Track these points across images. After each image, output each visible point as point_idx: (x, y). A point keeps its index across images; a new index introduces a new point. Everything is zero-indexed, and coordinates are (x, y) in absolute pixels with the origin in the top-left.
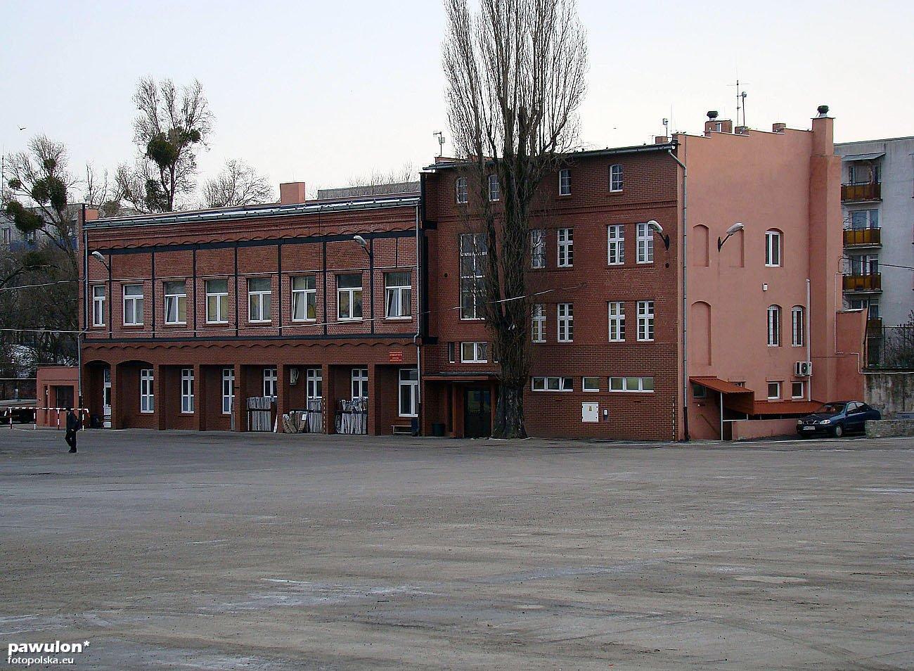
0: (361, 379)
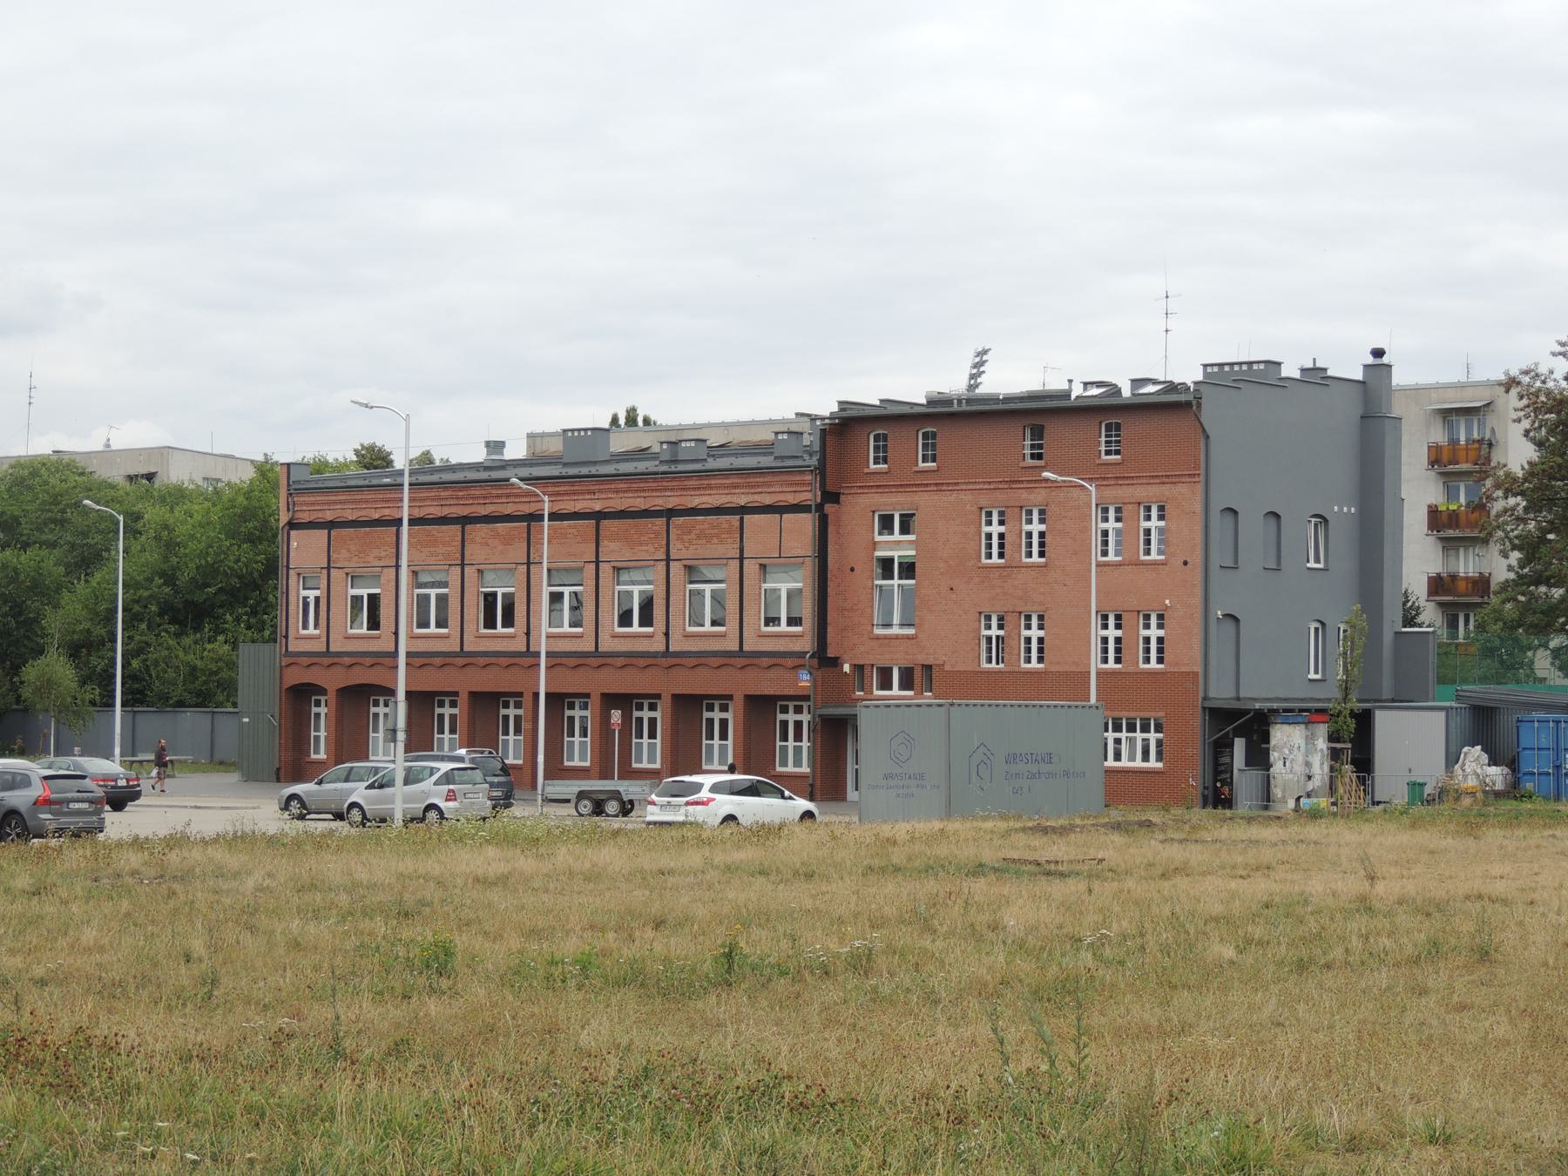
0: (447, 711)
